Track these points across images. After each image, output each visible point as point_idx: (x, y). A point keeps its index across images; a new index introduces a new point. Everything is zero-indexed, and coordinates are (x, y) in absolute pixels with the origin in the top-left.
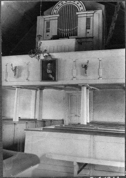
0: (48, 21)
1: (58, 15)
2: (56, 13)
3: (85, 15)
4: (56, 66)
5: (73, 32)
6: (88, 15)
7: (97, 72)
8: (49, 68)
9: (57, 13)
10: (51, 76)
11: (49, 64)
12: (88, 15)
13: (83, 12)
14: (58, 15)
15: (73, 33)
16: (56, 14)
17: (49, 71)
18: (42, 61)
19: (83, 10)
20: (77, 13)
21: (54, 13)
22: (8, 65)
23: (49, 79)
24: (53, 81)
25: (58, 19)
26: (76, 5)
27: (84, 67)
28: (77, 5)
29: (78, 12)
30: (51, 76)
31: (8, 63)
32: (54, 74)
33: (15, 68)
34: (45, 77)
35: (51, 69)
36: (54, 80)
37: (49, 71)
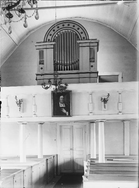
0: (42, 50)
1: (54, 43)
2: (50, 40)
3: (88, 44)
4: (71, 99)
5: (73, 65)
6: (91, 45)
7: (117, 106)
8: (62, 101)
9: (52, 40)
10: (64, 111)
11: (62, 97)
12: (91, 45)
13: (85, 40)
14: (54, 43)
15: (75, 65)
16: (51, 42)
17: (62, 105)
18: (53, 93)
19: (86, 38)
20: (78, 42)
21: (49, 40)
22: (8, 97)
23: (64, 115)
24: (67, 117)
25: (54, 48)
26: (76, 30)
27: (104, 101)
28: (74, 28)
29: (79, 40)
30: (64, 111)
31: (8, 96)
32: (68, 108)
33: (20, 101)
34: (57, 112)
35: (64, 102)
36: (67, 115)
37: (62, 104)
